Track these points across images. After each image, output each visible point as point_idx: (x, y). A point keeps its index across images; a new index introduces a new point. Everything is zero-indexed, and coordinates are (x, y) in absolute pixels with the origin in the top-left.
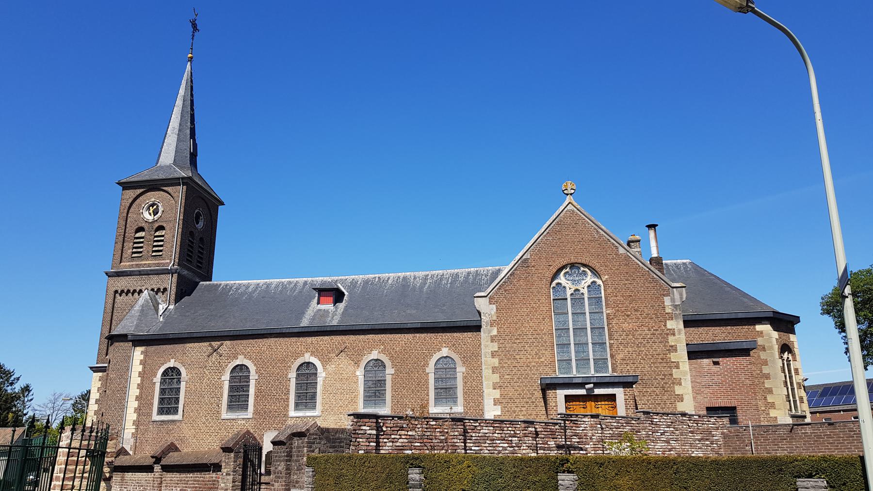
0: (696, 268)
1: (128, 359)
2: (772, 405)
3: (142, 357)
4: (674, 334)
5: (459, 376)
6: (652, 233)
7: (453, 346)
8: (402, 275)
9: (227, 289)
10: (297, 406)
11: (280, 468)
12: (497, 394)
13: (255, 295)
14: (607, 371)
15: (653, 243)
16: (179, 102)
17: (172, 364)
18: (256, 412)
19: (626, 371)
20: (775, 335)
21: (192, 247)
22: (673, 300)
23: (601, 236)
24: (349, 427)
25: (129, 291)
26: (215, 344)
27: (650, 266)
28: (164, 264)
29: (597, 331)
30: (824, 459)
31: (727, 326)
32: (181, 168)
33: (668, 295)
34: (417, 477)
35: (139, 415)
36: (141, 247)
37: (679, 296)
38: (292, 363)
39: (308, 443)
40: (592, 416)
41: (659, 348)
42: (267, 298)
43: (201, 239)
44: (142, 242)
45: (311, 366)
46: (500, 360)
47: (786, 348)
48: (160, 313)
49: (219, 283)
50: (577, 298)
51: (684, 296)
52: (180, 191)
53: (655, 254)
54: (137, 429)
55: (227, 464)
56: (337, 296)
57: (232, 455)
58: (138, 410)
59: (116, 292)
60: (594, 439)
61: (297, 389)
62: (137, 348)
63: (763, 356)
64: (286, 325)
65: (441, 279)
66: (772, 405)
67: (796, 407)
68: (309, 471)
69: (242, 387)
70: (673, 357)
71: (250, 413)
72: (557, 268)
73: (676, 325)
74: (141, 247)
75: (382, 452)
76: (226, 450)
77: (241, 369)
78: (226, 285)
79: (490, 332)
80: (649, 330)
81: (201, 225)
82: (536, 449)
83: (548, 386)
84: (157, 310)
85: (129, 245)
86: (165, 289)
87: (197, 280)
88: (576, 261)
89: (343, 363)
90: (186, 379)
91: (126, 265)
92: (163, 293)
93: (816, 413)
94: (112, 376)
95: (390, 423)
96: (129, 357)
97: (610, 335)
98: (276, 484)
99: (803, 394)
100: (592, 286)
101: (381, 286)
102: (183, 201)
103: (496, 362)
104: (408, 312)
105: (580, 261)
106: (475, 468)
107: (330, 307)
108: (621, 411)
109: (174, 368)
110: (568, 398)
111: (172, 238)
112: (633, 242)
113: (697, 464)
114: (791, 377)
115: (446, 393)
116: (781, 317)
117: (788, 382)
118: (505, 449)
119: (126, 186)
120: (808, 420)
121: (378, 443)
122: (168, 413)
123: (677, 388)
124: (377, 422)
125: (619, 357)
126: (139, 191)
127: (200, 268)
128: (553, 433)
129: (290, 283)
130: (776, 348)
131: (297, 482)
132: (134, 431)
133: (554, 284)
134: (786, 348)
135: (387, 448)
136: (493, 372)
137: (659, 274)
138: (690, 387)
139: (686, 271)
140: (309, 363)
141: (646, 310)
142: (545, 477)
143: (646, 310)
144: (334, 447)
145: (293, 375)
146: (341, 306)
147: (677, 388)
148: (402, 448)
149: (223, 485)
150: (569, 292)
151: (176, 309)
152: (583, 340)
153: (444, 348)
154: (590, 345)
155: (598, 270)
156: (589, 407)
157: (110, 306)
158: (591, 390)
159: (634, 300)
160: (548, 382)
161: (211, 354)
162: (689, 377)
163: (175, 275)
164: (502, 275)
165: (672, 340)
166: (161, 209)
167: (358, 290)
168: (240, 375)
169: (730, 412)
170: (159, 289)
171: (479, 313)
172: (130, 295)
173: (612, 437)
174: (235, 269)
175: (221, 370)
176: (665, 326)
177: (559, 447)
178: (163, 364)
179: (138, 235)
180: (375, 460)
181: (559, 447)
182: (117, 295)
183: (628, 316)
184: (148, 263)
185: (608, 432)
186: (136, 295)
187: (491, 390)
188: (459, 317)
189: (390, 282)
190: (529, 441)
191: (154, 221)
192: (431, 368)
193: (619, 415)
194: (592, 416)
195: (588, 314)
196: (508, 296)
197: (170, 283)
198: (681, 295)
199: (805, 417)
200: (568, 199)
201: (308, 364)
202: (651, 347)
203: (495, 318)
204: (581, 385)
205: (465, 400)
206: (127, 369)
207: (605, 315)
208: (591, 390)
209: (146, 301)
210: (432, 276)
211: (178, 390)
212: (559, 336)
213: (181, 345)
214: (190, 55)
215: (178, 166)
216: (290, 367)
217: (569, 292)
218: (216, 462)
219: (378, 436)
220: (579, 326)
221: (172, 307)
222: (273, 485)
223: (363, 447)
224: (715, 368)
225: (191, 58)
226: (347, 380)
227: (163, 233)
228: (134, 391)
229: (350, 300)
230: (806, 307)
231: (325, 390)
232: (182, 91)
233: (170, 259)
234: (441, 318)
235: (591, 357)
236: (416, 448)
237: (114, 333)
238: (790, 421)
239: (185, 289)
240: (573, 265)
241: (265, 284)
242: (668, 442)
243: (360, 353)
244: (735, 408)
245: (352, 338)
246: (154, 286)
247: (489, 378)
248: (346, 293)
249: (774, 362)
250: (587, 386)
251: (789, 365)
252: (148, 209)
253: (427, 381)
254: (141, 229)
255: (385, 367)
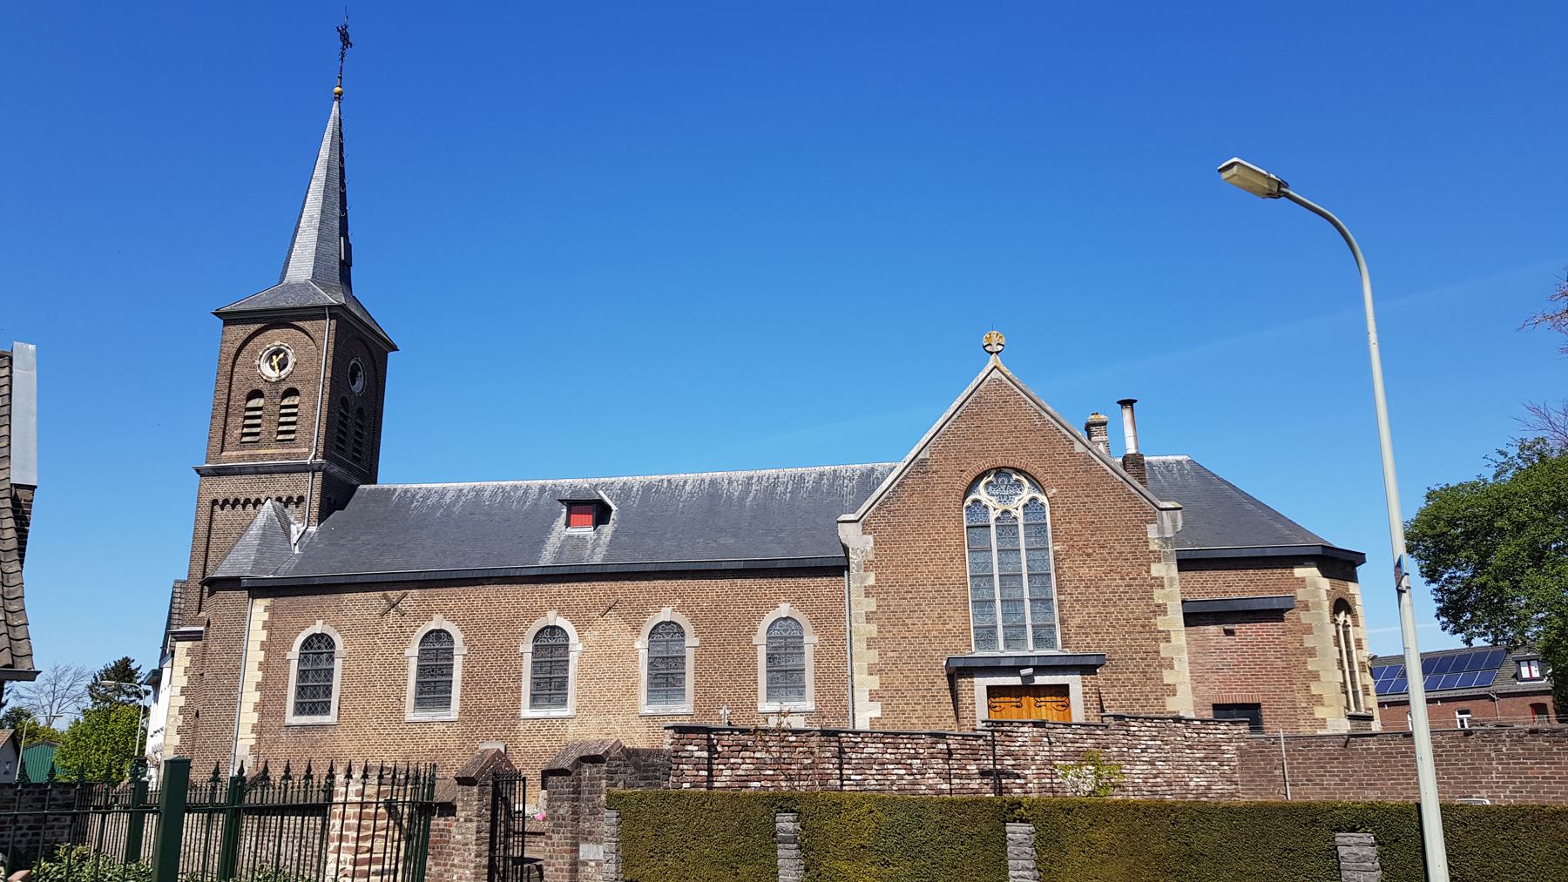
0: (1198, 470)
1: (242, 619)
2: (1319, 700)
3: (266, 616)
4: (1162, 586)
5: (809, 652)
6: (1127, 413)
7: (797, 601)
8: (707, 476)
9: (408, 497)
10: (535, 700)
11: (561, 811)
12: (874, 682)
13: (457, 509)
14: (1053, 646)
15: (1129, 431)
16: (320, 172)
17: (318, 627)
18: (464, 710)
19: (1085, 646)
20: (1325, 583)
21: (345, 426)
22: (1161, 530)
23: (1046, 423)
24: (667, 747)
25: (237, 501)
26: (393, 595)
27: (1124, 473)
28: (298, 456)
29: (1038, 580)
30: (1372, 807)
31: (1250, 568)
32: (326, 289)
33: (1152, 521)
34: (790, 826)
35: (262, 715)
36: (258, 426)
37: (1171, 523)
38: (527, 627)
39: (608, 772)
40: (1035, 724)
41: (1139, 608)
42: (476, 515)
43: (360, 411)
44: (259, 417)
45: (558, 634)
46: (881, 627)
47: (1342, 605)
48: (294, 539)
49: (392, 487)
50: (1006, 524)
51: (1180, 524)
52: (325, 330)
53: (1132, 450)
54: (259, 740)
55: (466, 803)
56: (600, 513)
57: (475, 789)
58: (260, 707)
59: (215, 502)
60: (1042, 766)
61: (534, 671)
62: (258, 601)
63: (1305, 618)
64: (515, 563)
65: (775, 485)
66: (1319, 700)
67: (1357, 702)
68: (611, 816)
69: (440, 667)
70: (1161, 623)
71: (454, 712)
72: (974, 474)
73: (1165, 570)
74: (258, 426)
75: (716, 784)
76: (464, 781)
77: (438, 638)
78: (406, 491)
79: (863, 580)
80: (1122, 579)
81: (358, 386)
82: (948, 778)
83: (959, 672)
84: (288, 534)
85: (236, 421)
86: (301, 499)
87: (355, 482)
88: (1005, 463)
89: (613, 626)
90: (344, 653)
91: (231, 457)
92: (297, 504)
93: (1390, 704)
94: (214, 647)
95: (727, 739)
96: (244, 616)
97: (1059, 587)
98: (555, 837)
99: (1369, 680)
100: (1031, 506)
101: (673, 496)
102: (331, 346)
103: (873, 629)
104: (722, 541)
105: (1011, 464)
106: (880, 814)
107: (588, 532)
108: (1078, 713)
109: (322, 635)
110: (992, 691)
111: (313, 409)
112: (1095, 425)
113: (1200, 813)
114: (1349, 653)
115: (785, 678)
116: (1335, 554)
117: (1345, 662)
118: (901, 777)
119: (230, 318)
120: (1376, 726)
121: (710, 770)
122: (312, 712)
123: (1165, 672)
124: (709, 739)
125: (1074, 622)
126: (253, 328)
127: (357, 460)
128: (974, 751)
129: (516, 488)
130: (1326, 605)
131: (590, 833)
132: (253, 742)
133: (968, 502)
134: (1342, 605)
135: (724, 778)
136: (869, 647)
137: (1140, 487)
138: (1187, 669)
139: (1182, 476)
140: (554, 627)
141: (1117, 546)
142: (985, 828)
143: (1117, 546)
144: (645, 778)
145: (527, 648)
146: (607, 530)
147: (1165, 672)
148: (744, 781)
149: (458, 837)
150: (993, 515)
151: (320, 532)
152: (1015, 595)
153: (783, 603)
154: (1027, 603)
155: (1041, 479)
156: (1025, 706)
157: (203, 527)
158: (1030, 677)
159: (1098, 529)
160: (960, 664)
161: (386, 612)
162: (1185, 656)
163: (319, 475)
164: (885, 485)
165: (1158, 596)
166: (291, 360)
167: (635, 503)
168: (436, 648)
169: (1250, 713)
170: (290, 499)
171: (846, 549)
172: (239, 507)
173: (1065, 756)
174: (421, 461)
175: (402, 639)
176: (1148, 572)
177: (984, 774)
178: (303, 629)
179: (252, 404)
180: (705, 802)
181: (984, 774)
182: (217, 508)
183: (1089, 555)
184: (271, 454)
185: (1059, 749)
186: (250, 507)
187: (865, 676)
188: (808, 551)
189: (688, 488)
190: (938, 764)
191: (280, 381)
192: (760, 638)
193: (1074, 720)
194: (1035, 724)
195: (1023, 552)
196: (894, 521)
197: (310, 487)
198: (1174, 521)
199: (1370, 718)
200: (993, 361)
201: (554, 629)
202: (1126, 606)
203: (871, 557)
204: (1013, 670)
205: (818, 691)
206: (240, 637)
207: (1051, 553)
208: (1030, 677)
209: (270, 519)
210: (760, 479)
211: (330, 672)
212: (976, 588)
213: (334, 597)
214: (338, 89)
215: (320, 285)
216: (522, 633)
217: (993, 515)
218: (445, 800)
219: (710, 759)
220: (1010, 570)
221: (313, 529)
222: (550, 838)
223: (688, 779)
224: (1227, 641)
225: (340, 94)
226: (619, 656)
227: (296, 400)
228: (252, 674)
229: (621, 520)
230: (1384, 539)
231: (582, 673)
232: (324, 153)
233: (309, 449)
234: (777, 553)
235: (1029, 622)
236: (767, 777)
237: (210, 575)
238: (1345, 727)
239: (335, 499)
240: (999, 471)
241: (473, 489)
242: (1152, 763)
243: (643, 612)
244: (1258, 706)
245: (628, 585)
246: (280, 494)
247: (863, 656)
248: (614, 508)
249: (1322, 628)
250: (1023, 672)
251: (1346, 634)
252: (270, 358)
253: (754, 659)
254: (257, 394)
255: (683, 634)
